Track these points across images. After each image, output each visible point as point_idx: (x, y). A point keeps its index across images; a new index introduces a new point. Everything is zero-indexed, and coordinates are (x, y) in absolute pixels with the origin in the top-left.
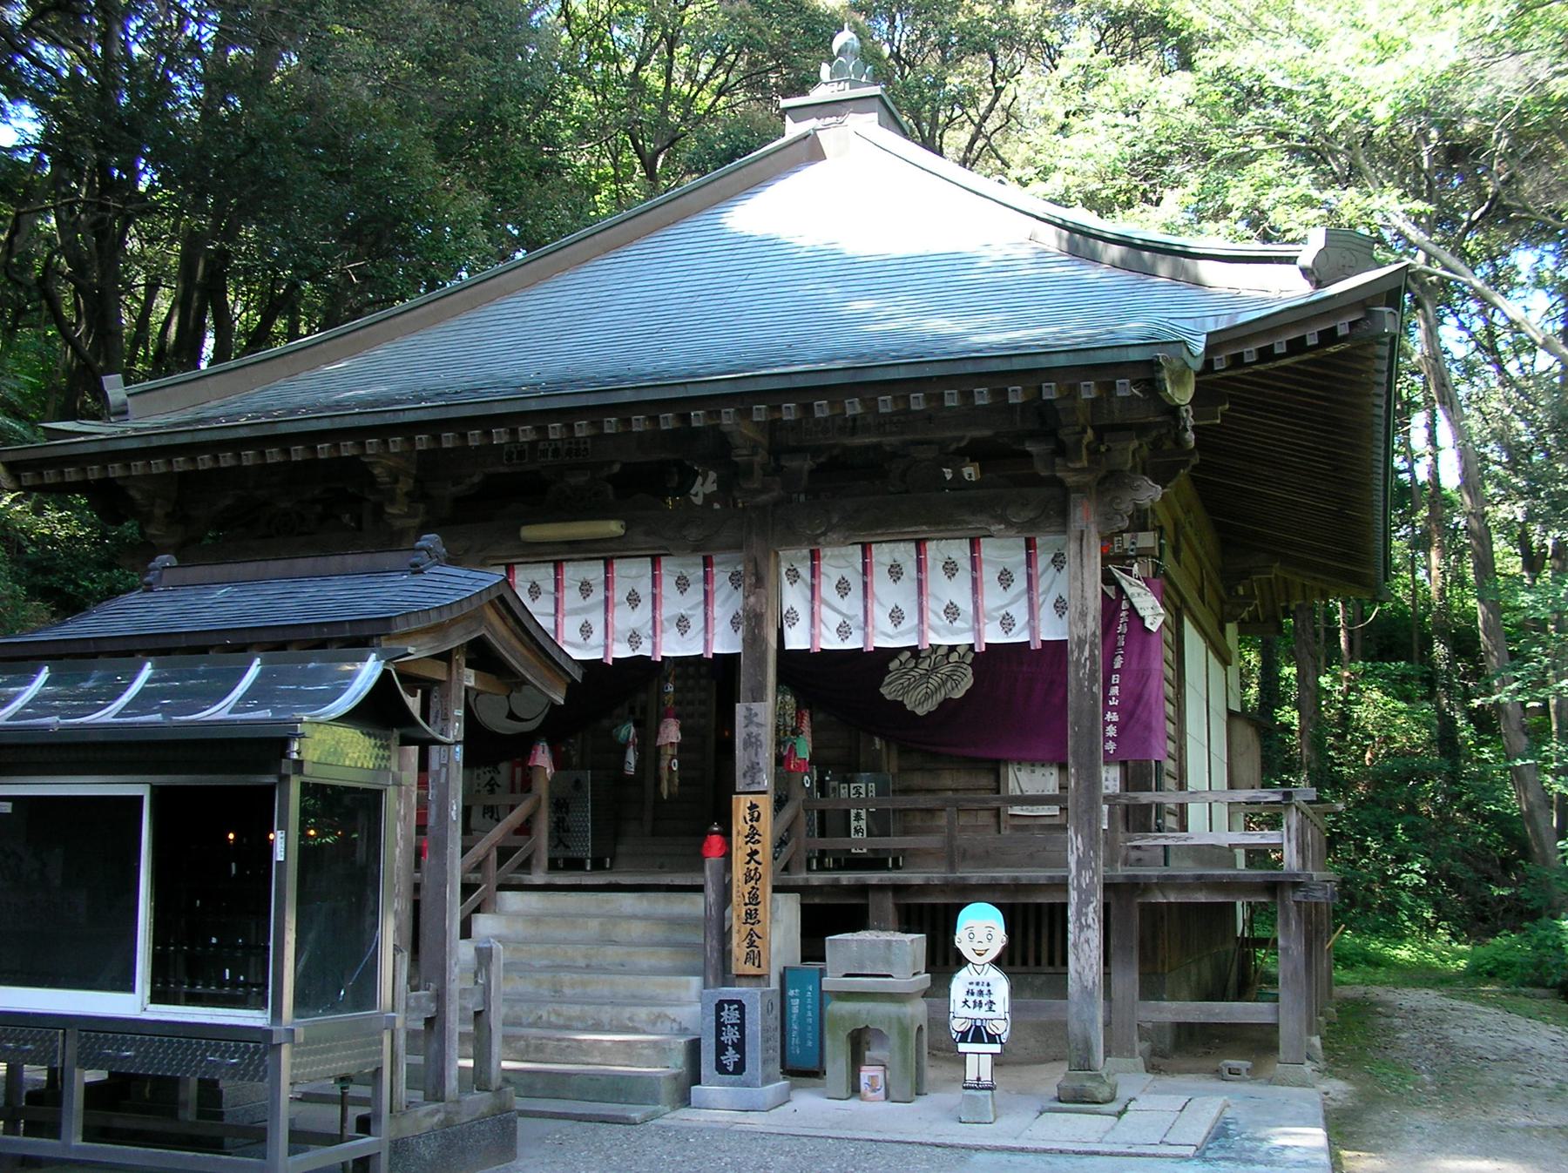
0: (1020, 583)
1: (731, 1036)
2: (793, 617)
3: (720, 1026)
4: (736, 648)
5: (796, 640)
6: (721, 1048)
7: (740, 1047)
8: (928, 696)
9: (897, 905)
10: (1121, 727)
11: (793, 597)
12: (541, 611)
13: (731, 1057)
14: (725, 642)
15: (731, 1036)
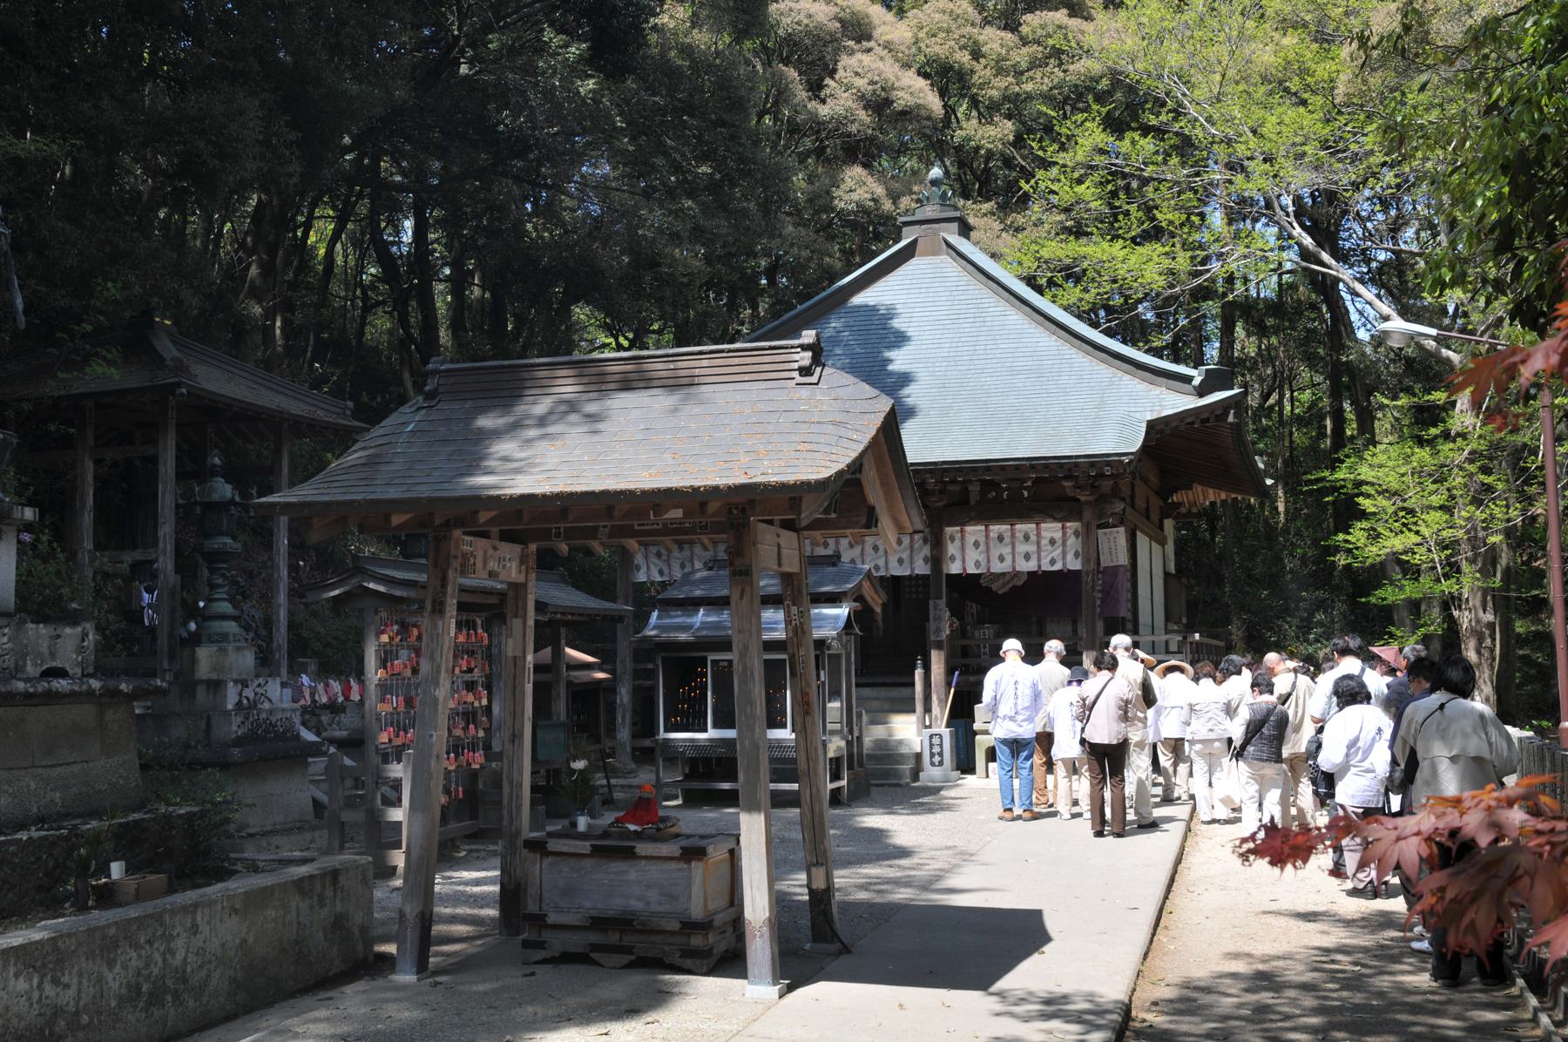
0: (982, 547)
1: (936, 750)
2: (638, 568)
3: (931, 745)
4: (928, 572)
5: (955, 568)
6: (932, 755)
7: (941, 754)
8: (1004, 585)
9: (799, 514)
10: (1103, 600)
11: (952, 549)
12: (524, 485)
13: (937, 759)
14: (922, 568)
15: (936, 750)
